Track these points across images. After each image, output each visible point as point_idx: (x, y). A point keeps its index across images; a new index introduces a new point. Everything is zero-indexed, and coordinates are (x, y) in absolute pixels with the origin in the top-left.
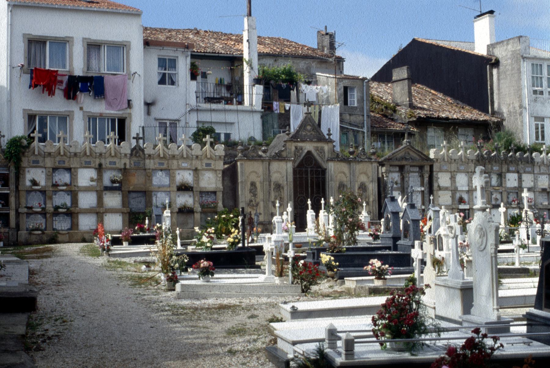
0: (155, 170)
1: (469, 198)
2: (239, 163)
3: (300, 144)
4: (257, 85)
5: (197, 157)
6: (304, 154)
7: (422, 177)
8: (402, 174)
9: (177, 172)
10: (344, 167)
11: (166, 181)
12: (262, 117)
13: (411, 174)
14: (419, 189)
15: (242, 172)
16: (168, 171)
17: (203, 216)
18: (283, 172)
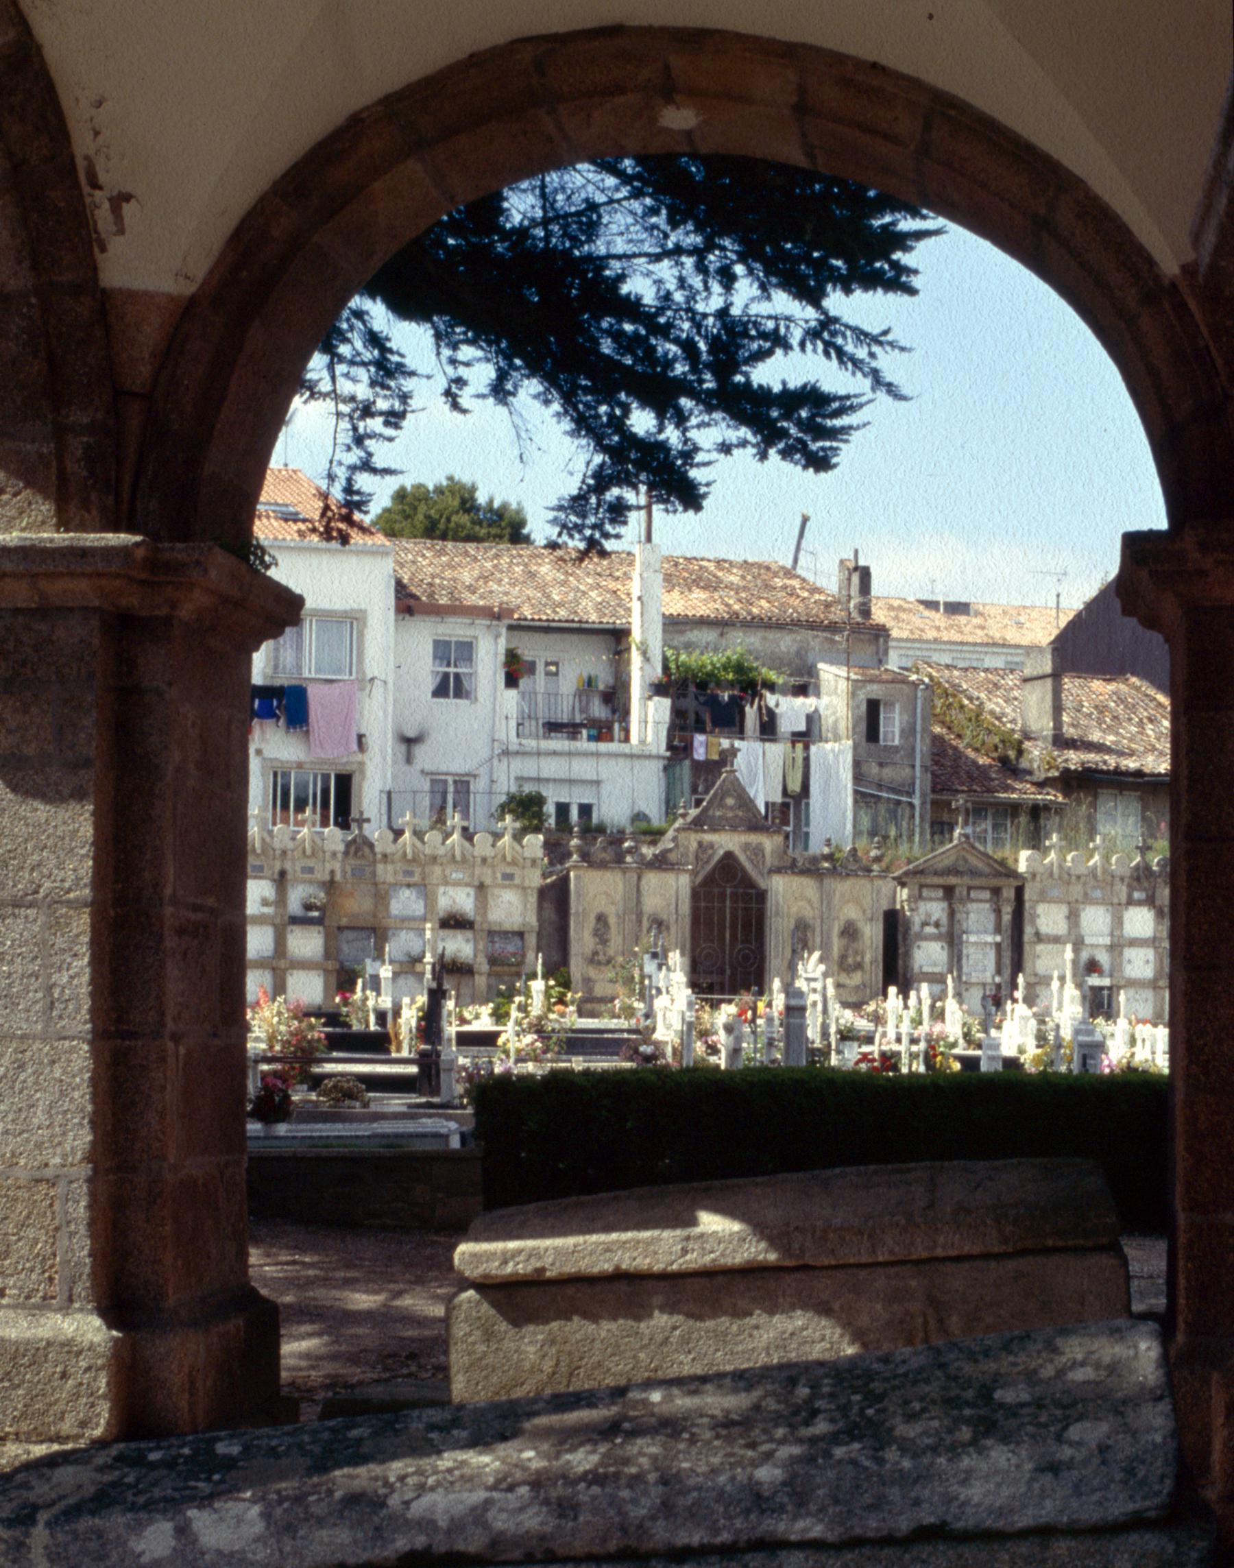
0: (397, 885)
1: (1113, 960)
2: (572, 874)
3: (708, 837)
4: (656, 699)
5: (484, 860)
6: (716, 858)
7: (998, 912)
8: (950, 905)
9: (441, 889)
10: (808, 886)
11: (418, 908)
12: (665, 769)
13: (973, 907)
14: (989, 939)
15: (579, 895)
16: (425, 890)
17: (493, 981)
18: (669, 892)
